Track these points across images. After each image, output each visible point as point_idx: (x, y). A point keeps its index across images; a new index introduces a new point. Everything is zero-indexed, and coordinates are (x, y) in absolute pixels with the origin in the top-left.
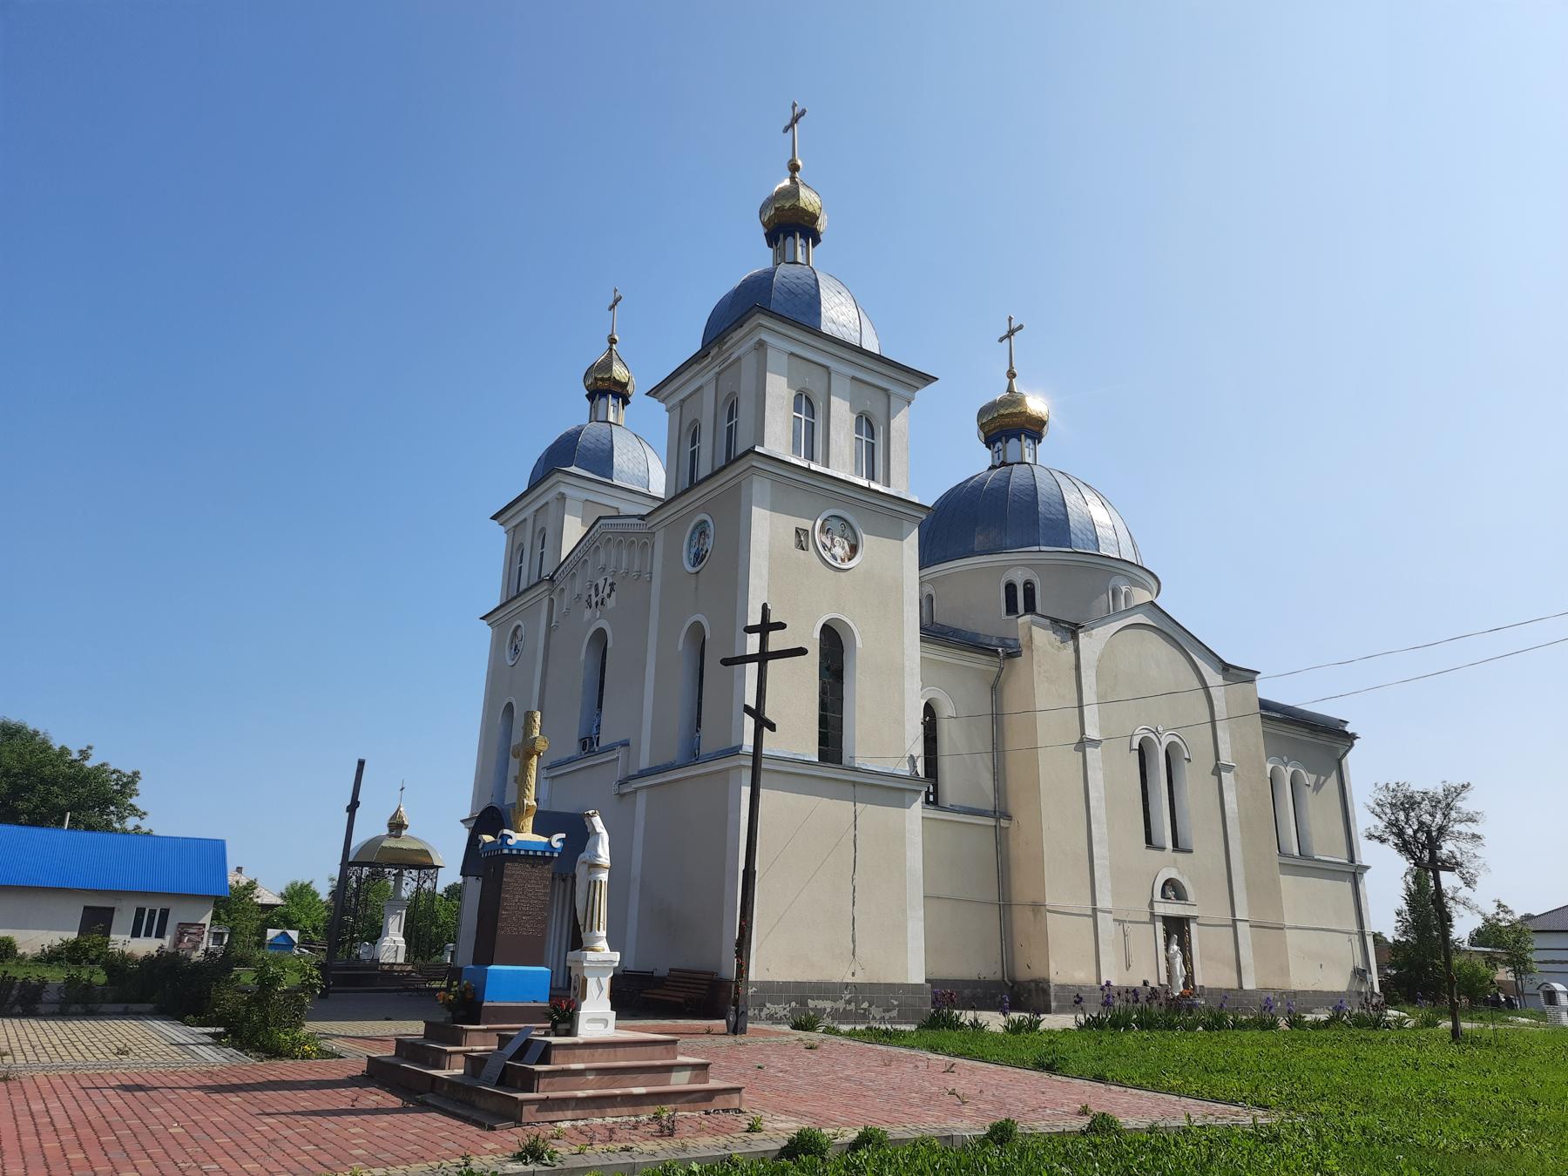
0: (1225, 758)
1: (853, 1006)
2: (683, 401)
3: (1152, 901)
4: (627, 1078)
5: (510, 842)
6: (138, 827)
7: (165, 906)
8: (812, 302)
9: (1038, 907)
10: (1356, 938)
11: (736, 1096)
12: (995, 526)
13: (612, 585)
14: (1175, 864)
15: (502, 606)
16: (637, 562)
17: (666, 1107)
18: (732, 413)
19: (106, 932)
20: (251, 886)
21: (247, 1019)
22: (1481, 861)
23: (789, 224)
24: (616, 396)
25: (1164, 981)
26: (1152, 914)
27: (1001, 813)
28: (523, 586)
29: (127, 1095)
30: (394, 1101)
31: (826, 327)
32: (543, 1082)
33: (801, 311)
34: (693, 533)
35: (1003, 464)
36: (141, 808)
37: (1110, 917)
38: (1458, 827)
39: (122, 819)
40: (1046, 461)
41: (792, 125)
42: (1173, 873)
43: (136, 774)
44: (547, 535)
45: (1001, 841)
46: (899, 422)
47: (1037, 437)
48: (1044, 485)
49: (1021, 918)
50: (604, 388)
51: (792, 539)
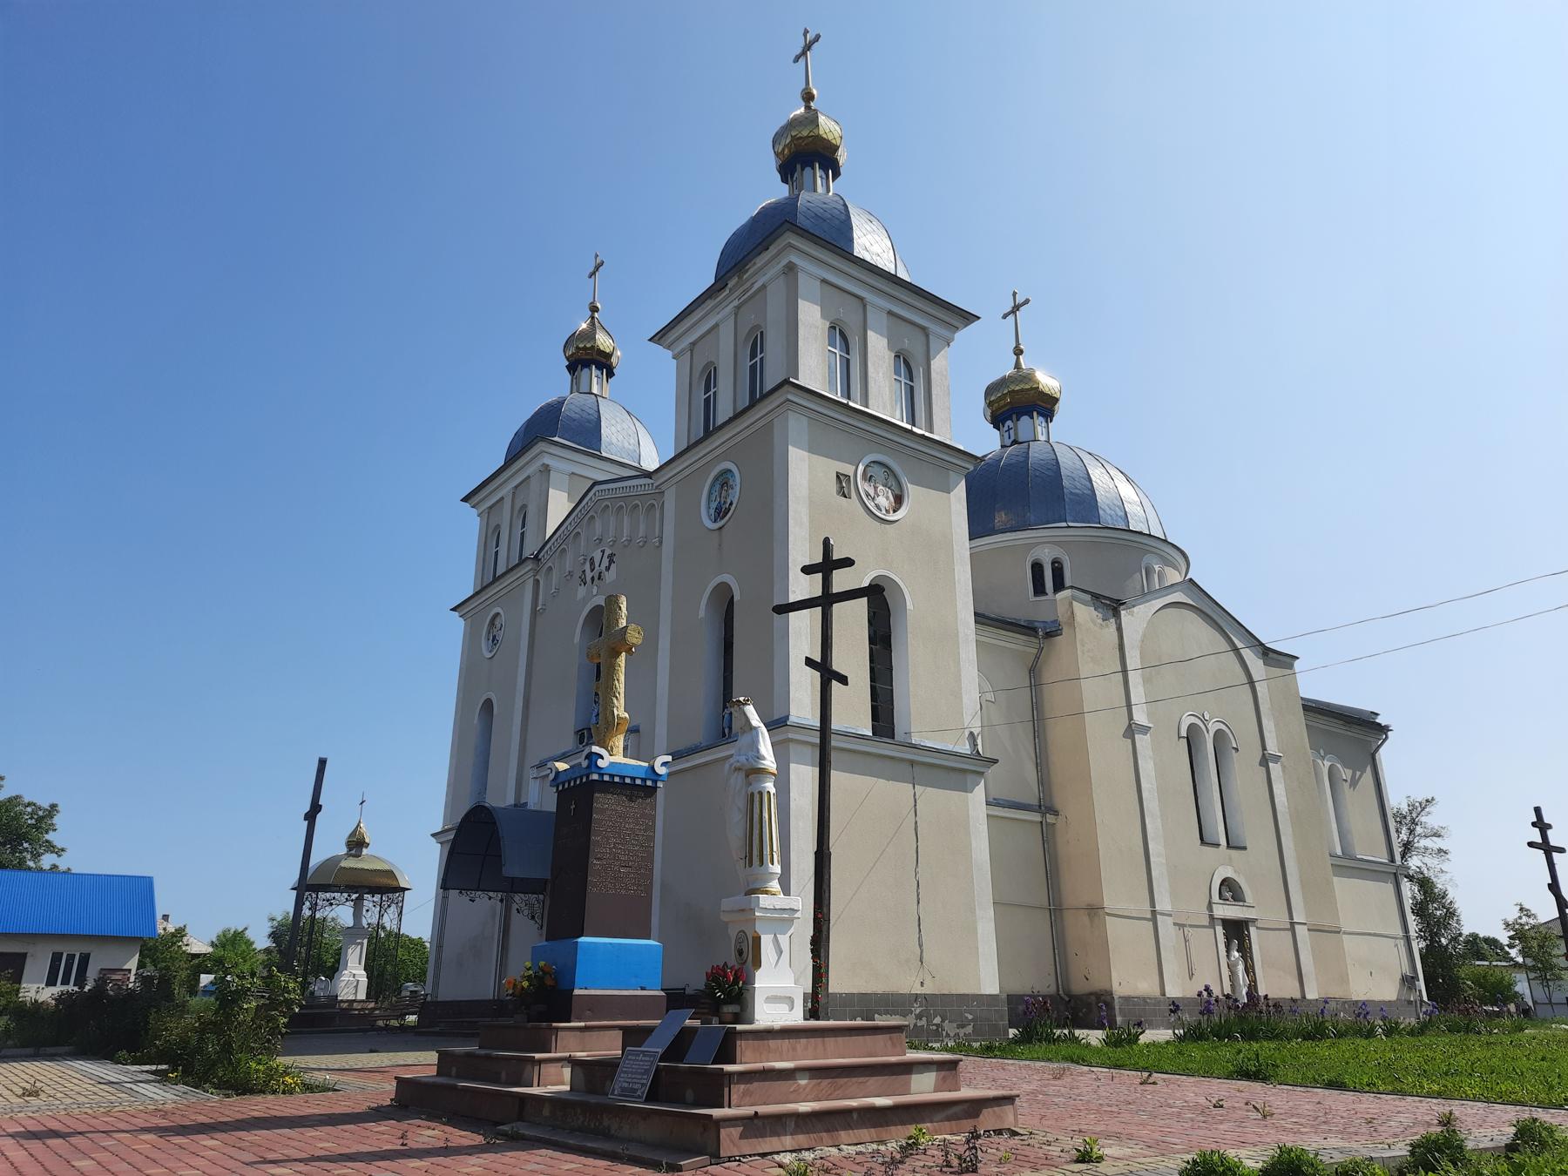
0: (1272, 749)
1: (924, 1022)
2: (693, 344)
3: (1210, 904)
4: (853, 1083)
5: (600, 763)
6: (55, 867)
7: (85, 950)
8: (843, 228)
9: (1095, 911)
10: (1401, 943)
11: (1008, 1109)
12: (1019, 492)
13: (611, 556)
14: (1230, 862)
15: (476, 594)
16: (642, 527)
17: (925, 1126)
18: (756, 345)
19: (17, 978)
20: (180, 933)
21: (199, 1050)
22: (1448, 876)
23: (805, 154)
24: (600, 367)
25: (1227, 990)
26: (1212, 917)
27: (1046, 807)
28: (501, 570)
29: (34, 1146)
30: (478, 1139)
31: (858, 251)
32: (737, 1090)
33: (834, 236)
34: (713, 485)
35: (1015, 442)
36: (58, 844)
37: (1170, 920)
38: (1423, 843)
39: (36, 856)
40: (1062, 436)
41: (804, 53)
42: (1228, 873)
43: (53, 806)
44: (527, 512)
45: (1047, 837)
46: (937, 364)
47: (1048, 415)
48: (1066, 460)
49: (1076, 925)
50: (586, 358)
51: (834, 487)
